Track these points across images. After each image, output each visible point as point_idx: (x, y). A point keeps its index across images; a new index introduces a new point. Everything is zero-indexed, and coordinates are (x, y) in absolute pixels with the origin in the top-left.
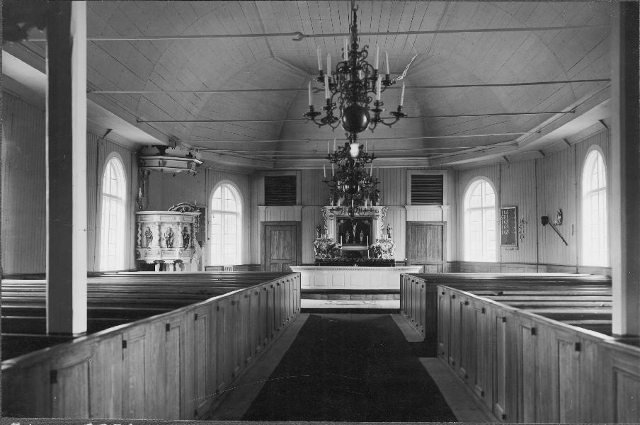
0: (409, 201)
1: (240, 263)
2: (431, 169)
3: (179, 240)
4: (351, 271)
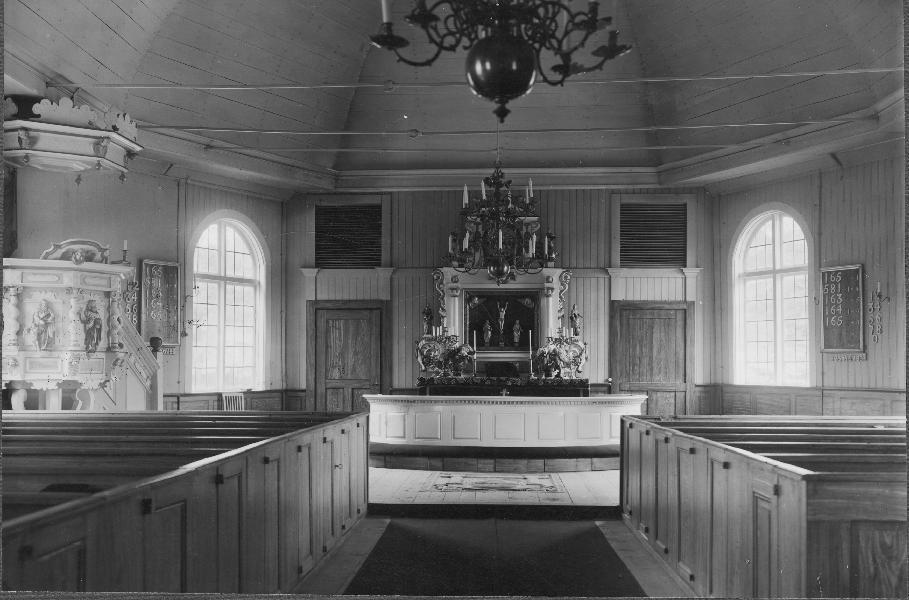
0: (616, 257)
1: (260, 387)
2: (662, 191)
3: (71, 333)
4: (494, 407)
